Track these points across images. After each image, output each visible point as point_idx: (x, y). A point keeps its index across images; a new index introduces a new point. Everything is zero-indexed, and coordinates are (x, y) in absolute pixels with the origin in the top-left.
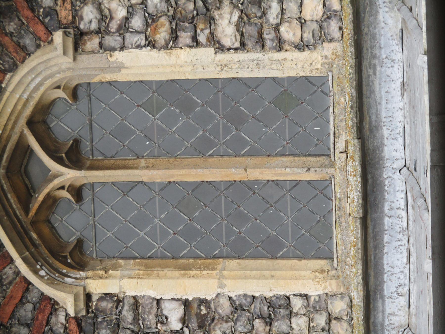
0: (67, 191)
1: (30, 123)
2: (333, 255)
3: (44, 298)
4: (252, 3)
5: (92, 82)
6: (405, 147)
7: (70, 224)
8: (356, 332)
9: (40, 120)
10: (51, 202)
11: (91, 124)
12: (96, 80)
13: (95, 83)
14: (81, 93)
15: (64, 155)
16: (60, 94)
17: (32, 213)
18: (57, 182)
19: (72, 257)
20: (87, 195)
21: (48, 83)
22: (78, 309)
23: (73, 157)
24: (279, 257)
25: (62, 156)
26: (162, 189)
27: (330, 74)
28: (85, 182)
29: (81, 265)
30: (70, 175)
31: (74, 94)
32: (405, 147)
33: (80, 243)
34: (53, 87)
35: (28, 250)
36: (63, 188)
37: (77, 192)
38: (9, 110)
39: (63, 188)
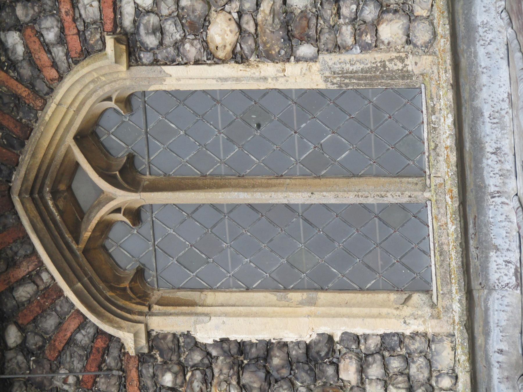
0: (124, 215)
1: (79, 138)
2: (431, 286)
3: (99, 332)
4: (265, 390)
5: (149, 90)
6: (516, 177)
7: (128, 248)
8: (460, 385)
9: (88, 137)
10: (105, 226)
11: (147, 138)
12: (152, 88)
13: (152, 91)
14: (137, 103)
15: (117, 173)
16: (111, 104)
17: (87, 234)
18: (112, 205)
19: (132, 291)
20: (145, 216)
21: (94, 98)
22: (139, 346)
23: (128, 175)
24: (368, 289)
25: (116, 174)
26: (231, 211)
27: (423, 86)
28: (144, 203)
29: (143, 298)
30: (124, 198)
31: (127, 102)
32: (516, 177)
33: (140, 273)
34: (101, 99)
35: (80, 280)
36: (117, 210)
37: (135, 215)
38: (55, 127)
39: (117, 210)
